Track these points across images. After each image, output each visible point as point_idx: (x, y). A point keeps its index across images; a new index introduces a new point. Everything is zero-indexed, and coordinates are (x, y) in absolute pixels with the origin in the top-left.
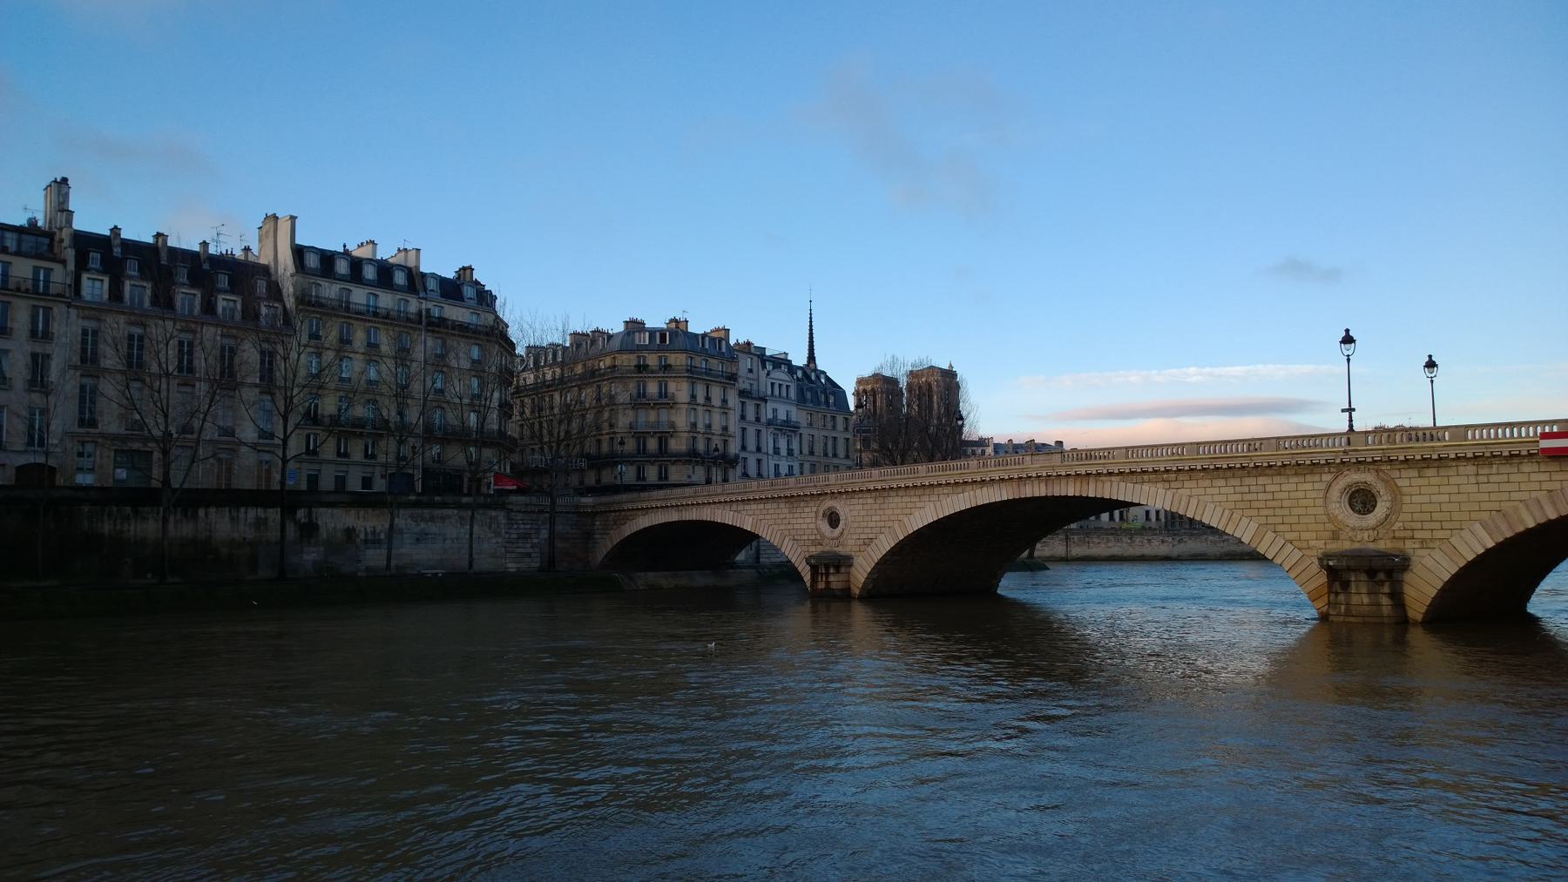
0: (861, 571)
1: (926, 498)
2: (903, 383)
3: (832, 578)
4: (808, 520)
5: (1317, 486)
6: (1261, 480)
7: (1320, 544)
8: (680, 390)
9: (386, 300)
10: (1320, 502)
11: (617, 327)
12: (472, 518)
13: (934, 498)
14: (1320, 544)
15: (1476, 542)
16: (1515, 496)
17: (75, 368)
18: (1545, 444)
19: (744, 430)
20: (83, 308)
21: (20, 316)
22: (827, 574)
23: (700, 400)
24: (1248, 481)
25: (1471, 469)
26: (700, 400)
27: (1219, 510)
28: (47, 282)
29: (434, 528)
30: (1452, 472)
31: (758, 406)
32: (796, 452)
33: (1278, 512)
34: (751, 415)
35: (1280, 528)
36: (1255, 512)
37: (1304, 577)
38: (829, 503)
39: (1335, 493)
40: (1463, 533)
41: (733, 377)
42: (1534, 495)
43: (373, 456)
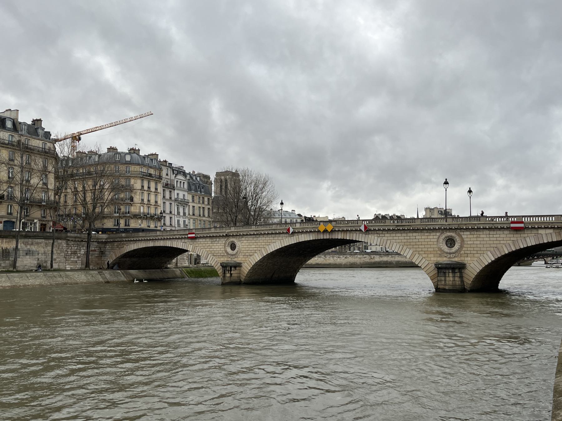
0: (246, 268)
1: (276, 238)
2: (212, 178)
3: (232, 272)
4: (220, 246)
5: (434, 237)
6: (414, 234)
7: (435, 259)
8: (137, 184)
10: (435, 243)
11: (104, 150)
12: (53, 244)
13: (280, 238)
14: (435, 259)
15: (489, 258)
16: (502, 242)
18: (512, 225)
19: (164, 203)
22: (231, 270)
23: (146, 188)
24: (409, 234)
25: (488, 232)
26: (146, 188)
27: (398, 246)
29: (34, 248)
30: (481, 233)
31: (170, 191)
32: (187, 214)
33: (420, 246)
34: (167, 196)
35: (420, 252)
36: (412, 247)
37: (429, 271)
38: (232, 239)
39: (441, 240)
40: (485, 255)
41: (160, 177)
42: (508, 242)
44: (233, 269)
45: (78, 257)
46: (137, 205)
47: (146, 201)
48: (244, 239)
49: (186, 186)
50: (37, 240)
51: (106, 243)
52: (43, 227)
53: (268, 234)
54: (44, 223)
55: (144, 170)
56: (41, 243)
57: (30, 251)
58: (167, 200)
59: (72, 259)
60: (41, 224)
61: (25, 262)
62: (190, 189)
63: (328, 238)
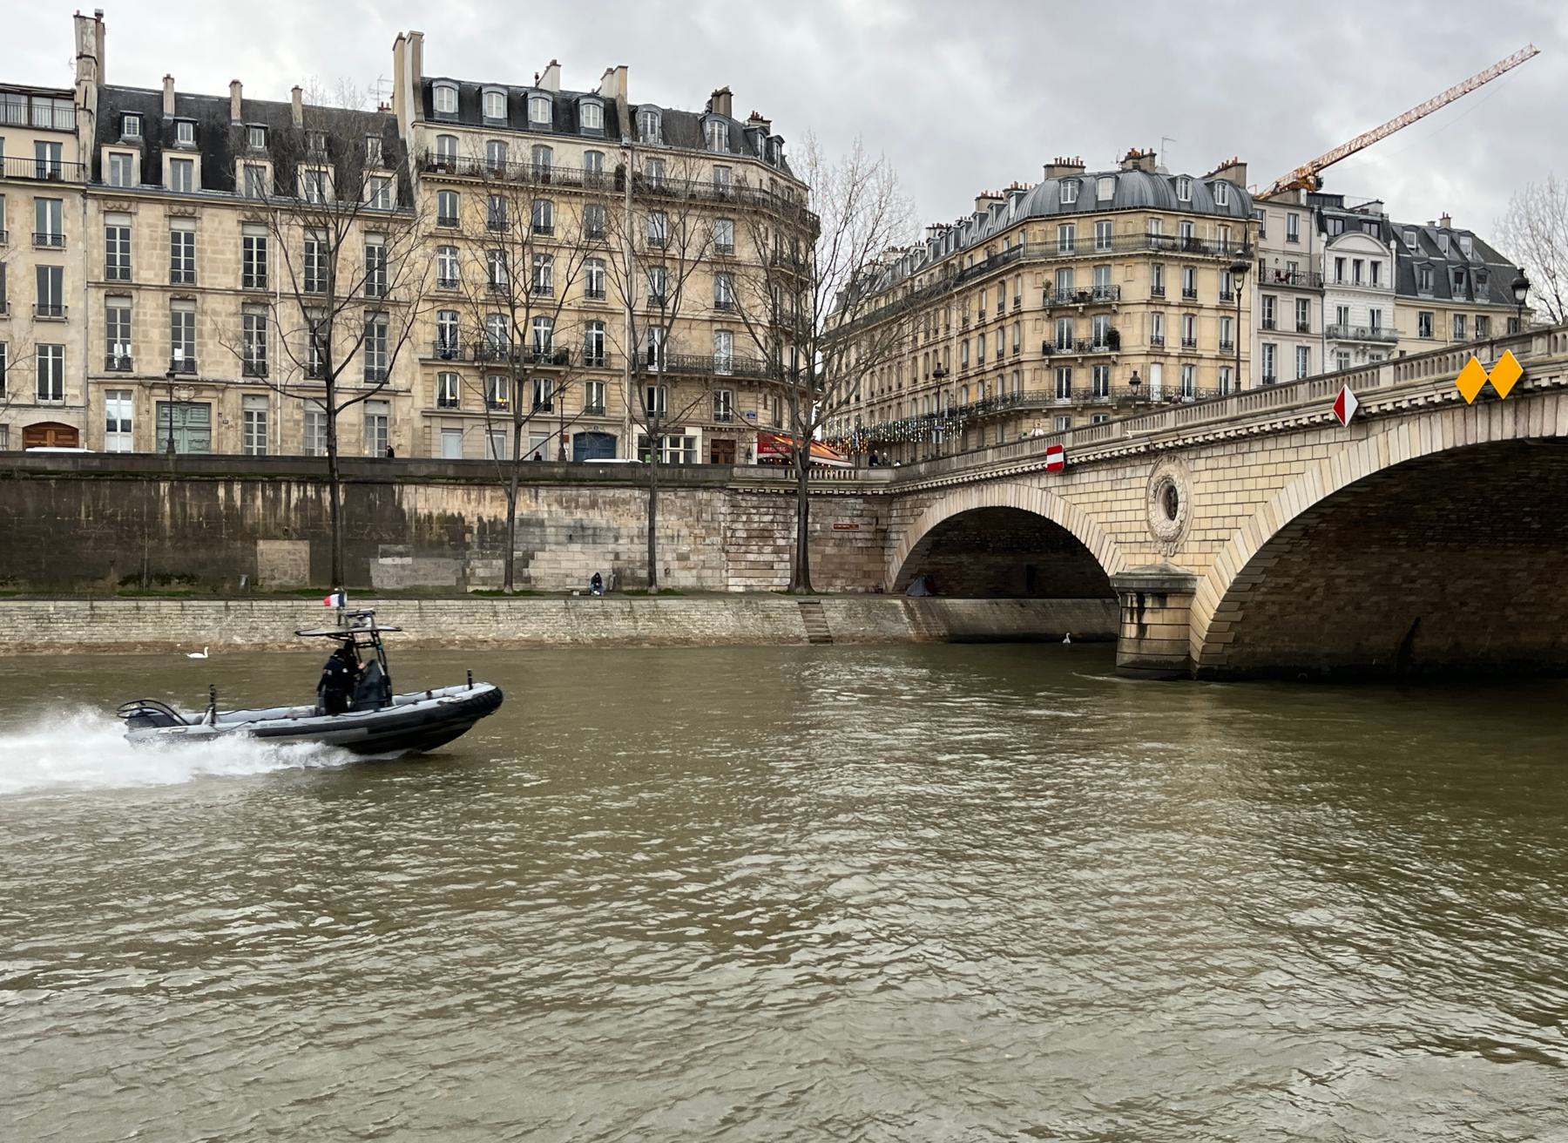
1: (1306, 453)
8: (1133, 282)
9: (469, 148)
13: (1320, 452)
17: (98, 285)
20: (106, 198)
21: (20, 216)
22: (1141, 610)
28: (56, 162)
29: (597, 518)
38: (1168, 468)
43: (548, 407)
44: (1149, 603)
45: (778, 551)
46: (1132, 360)
47: (1173, 344)
48: (1201, 464)
49: (1387, 276)
50: (610, 493)
51: (889, 499)
52: (722, 452)
53: (1276, 433)
54: (723, 437)
55: (1169, 227)
56: (626, 502)
57: (583, 528)
58: (1285, 334)
59: (751, 557)
60: (715, 443)
61: (564, 564)
62: (1407, 285)
63: (1509, 435)
